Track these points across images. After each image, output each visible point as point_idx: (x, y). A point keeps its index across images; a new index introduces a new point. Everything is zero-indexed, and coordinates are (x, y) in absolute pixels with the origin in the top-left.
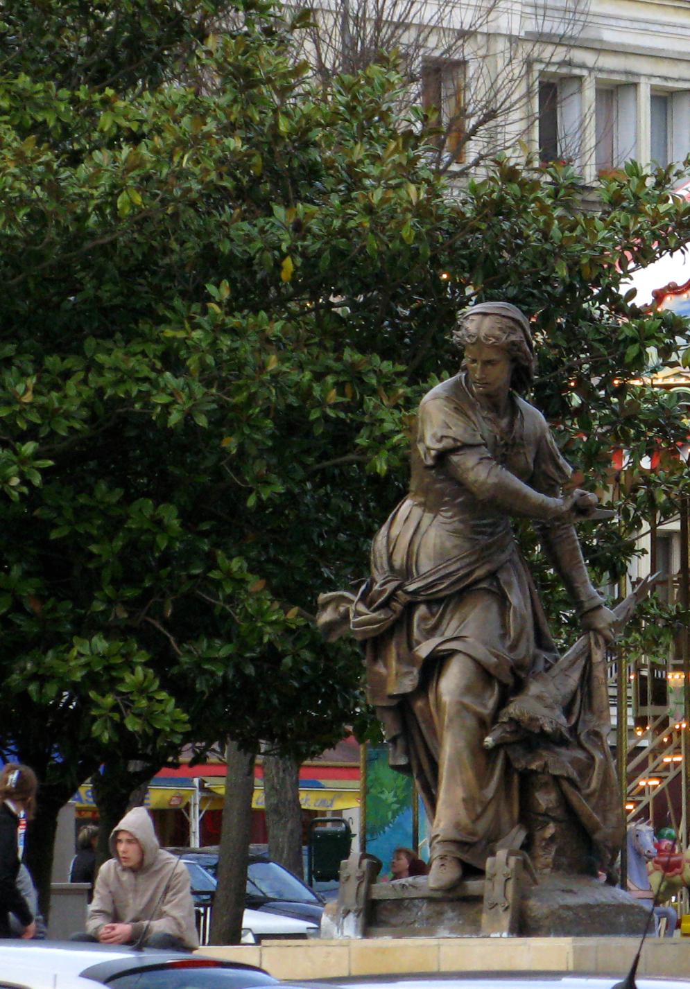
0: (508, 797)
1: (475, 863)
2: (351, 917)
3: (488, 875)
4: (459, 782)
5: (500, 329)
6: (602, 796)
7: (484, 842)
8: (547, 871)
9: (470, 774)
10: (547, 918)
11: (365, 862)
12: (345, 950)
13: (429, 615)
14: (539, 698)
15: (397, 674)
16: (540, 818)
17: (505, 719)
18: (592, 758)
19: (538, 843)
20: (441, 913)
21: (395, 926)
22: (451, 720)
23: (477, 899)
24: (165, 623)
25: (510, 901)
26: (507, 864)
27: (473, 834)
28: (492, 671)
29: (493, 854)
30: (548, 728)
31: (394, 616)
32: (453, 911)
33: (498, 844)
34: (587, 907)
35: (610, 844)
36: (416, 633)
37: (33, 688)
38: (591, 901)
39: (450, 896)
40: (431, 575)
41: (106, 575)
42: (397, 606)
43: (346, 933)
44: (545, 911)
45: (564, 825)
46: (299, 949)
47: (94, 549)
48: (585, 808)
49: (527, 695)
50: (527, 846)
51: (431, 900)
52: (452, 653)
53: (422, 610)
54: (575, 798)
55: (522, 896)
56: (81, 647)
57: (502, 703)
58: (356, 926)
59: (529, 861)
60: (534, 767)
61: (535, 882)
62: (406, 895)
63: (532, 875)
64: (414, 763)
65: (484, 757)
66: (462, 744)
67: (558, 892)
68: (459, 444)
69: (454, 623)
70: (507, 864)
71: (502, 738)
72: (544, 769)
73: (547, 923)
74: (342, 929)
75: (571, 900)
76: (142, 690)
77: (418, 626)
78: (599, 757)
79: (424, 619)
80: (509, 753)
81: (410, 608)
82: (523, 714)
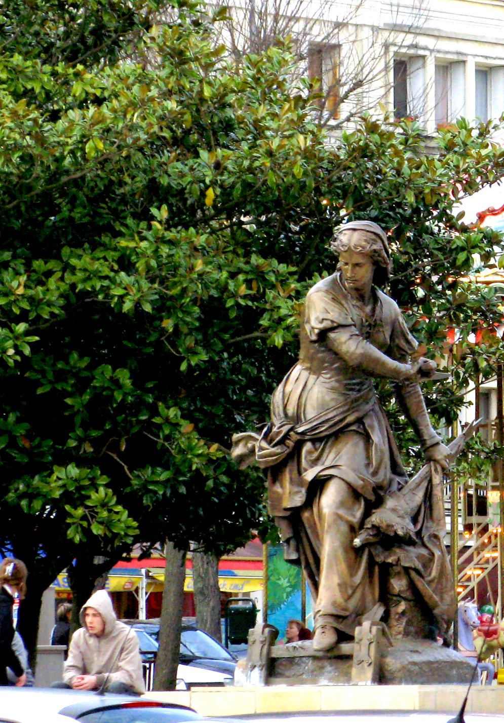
1: (347, 631)
2: (257, 670)
3: (356, 640)
6: (439, 582)
7: (354, 616)
8: (400, 636)
9: (343, 566)
10: (400, 671)
11: (267, 630)
13: (313, 450)
14: (394, 510)
15: (290, 493)
16: (395, 598)
17: (369, 526)
18: (433, 554)
19: (392, 616)
20: (322, 668)
21: (288, 677)
22: (329, 527)
23: (348, 657)
25: (373, 658)
26: (370, 631)
27: (345, 609)
28: (359, 490)
29: (360, 624)
30: (400, 532)
31: (288, 451)
32: (331, 666)
33: (364, 617)
34: (429, 663)
35: (445, 617)
36: (304, 463)
37: (24, 503)
38: (432, 659)
39: (329, 655)
40: (314, 421)
41: (78, 420)
42: (290, 443)
45: (412, 603)
48: (427, 590)
49: (385, 508)
50: (385, 618)
51: (315, 658)
52: (331, 477)
53: (308, 446)
54: (420, 584)
55: (381, 655)
56: (59, 473)
57: (367, 514)
58: (260, 677)
59: (386, 629)
60: (390, 560)
61: (391, 645)
62: (297, 654)
63: (388, 639)
64: (302, 558)
66: (337, 544)
68: (335, 325)
69: (332, 456)
70: (370, 631)
71: (367, 540)
73: (399, 674)
75: (417, 658)
76: (104, 505)
77: (306, 457)
78: (437, 553)
79: (309, 453)
80: (372, 550)
81: (299, 445)
82: (382, 522)
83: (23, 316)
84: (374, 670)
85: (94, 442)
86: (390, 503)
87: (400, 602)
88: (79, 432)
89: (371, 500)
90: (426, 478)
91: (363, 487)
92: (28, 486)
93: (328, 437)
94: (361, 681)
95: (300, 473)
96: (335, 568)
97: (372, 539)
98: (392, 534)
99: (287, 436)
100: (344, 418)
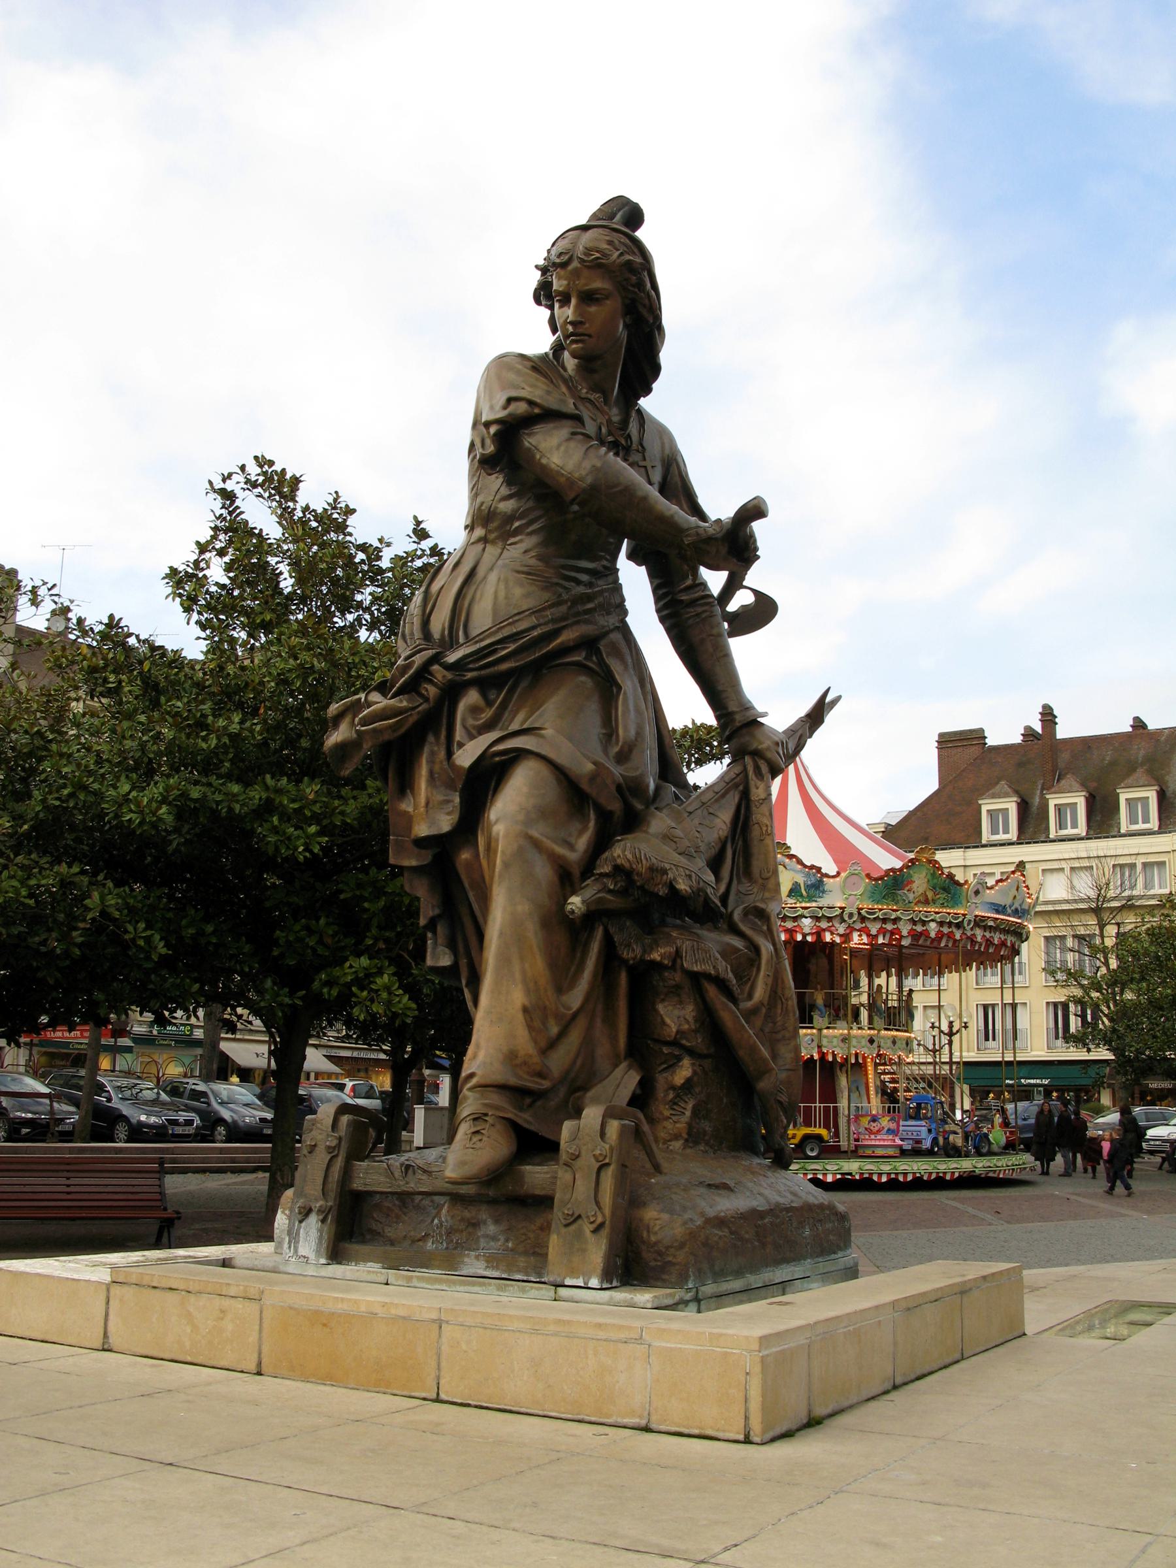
0: (610, 1020)
1: (545, 1132)
2: (313, 1219)
3: (563, 1156)
4: (518, 976)
5: (610, 243)
6: (770, 1017)
7: (562, 1091)
8: (677, 1145)
9: (538, 965)
10: (682, 1246)
11: (345, 1119)
12: (253, 1307)
13: (482, 703)
14: (667, 838)
15: (427, 804)
16: (665, 1050)
17: (607, 869)
18: (757, 950)
19: (660, 1094)
20: (475, 1224)
21: (392, 1243)
22: (506, 865)
23: (544, 1202)
24: (409, 953)
25: (607, 1211)
26: (603, 1134)
27: (541, 1075)
28: (585, 786)
29: (577, 1113)
30: (682, 886)
31: (425, 706)
32: (497, 1222)
33: (590, 1094)
34: (753, 1215)
35: (784, 1098)
36: (459, 734)
37: (325, 990)
38: (759, 1204)
39: (491, 1193)
41: (375, 922)
42: (432, 691)
43: (302, 1251)
44: (678, 1231)
45: (707, 1063)
46: (170, 1294)
47: (366, 905)
48: (746, 1034)
49: (646, 832)
50: (641, 1099)
51: (457, 1199)
52: (519, 755)
53: (473, 696)
54: (728, 1014)
55: (631, 1199)
56: (352, 961)
57: (601, 844)
58: (320, 1238)
59: (646, 1127)
60: (655, 956)
61: (657, 1168)
62: (412, 1186)
63: (650, 1155)
64: (463, 962)
65: (566, 935)
66: (524, 908)
67: (703, 1190)
68: (537, 411)
69: (520, 717)
70: (603, 1134)
71: (600, 901)
72: (674, 961)
73: (681, 1256)
74: (297, 1242)
75: (726, 1205)
76: (388, 988)
77: (464, 720)
78: (766, 948)
79: (474, 710)
80: (612, 930)
81: (452, 693)
82: (639, 861)
83: (316, 818)
84: (611, 1246)
85: (386, 941)
86: (659, 822)
87: (679, 1059)
88: (374, 931)
89: (611, 813)
90: (736, 786)
91: (593, 778)
92: (327, 975)
93: (515, 675)
94: (573, 1273)
95: (450, 754)
96: (516, 968)
97: (614, 902)
98: (662, 891)
99: (423, 674)
100: (556, 633)
